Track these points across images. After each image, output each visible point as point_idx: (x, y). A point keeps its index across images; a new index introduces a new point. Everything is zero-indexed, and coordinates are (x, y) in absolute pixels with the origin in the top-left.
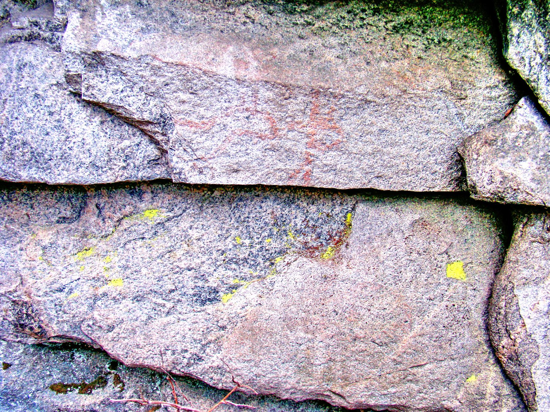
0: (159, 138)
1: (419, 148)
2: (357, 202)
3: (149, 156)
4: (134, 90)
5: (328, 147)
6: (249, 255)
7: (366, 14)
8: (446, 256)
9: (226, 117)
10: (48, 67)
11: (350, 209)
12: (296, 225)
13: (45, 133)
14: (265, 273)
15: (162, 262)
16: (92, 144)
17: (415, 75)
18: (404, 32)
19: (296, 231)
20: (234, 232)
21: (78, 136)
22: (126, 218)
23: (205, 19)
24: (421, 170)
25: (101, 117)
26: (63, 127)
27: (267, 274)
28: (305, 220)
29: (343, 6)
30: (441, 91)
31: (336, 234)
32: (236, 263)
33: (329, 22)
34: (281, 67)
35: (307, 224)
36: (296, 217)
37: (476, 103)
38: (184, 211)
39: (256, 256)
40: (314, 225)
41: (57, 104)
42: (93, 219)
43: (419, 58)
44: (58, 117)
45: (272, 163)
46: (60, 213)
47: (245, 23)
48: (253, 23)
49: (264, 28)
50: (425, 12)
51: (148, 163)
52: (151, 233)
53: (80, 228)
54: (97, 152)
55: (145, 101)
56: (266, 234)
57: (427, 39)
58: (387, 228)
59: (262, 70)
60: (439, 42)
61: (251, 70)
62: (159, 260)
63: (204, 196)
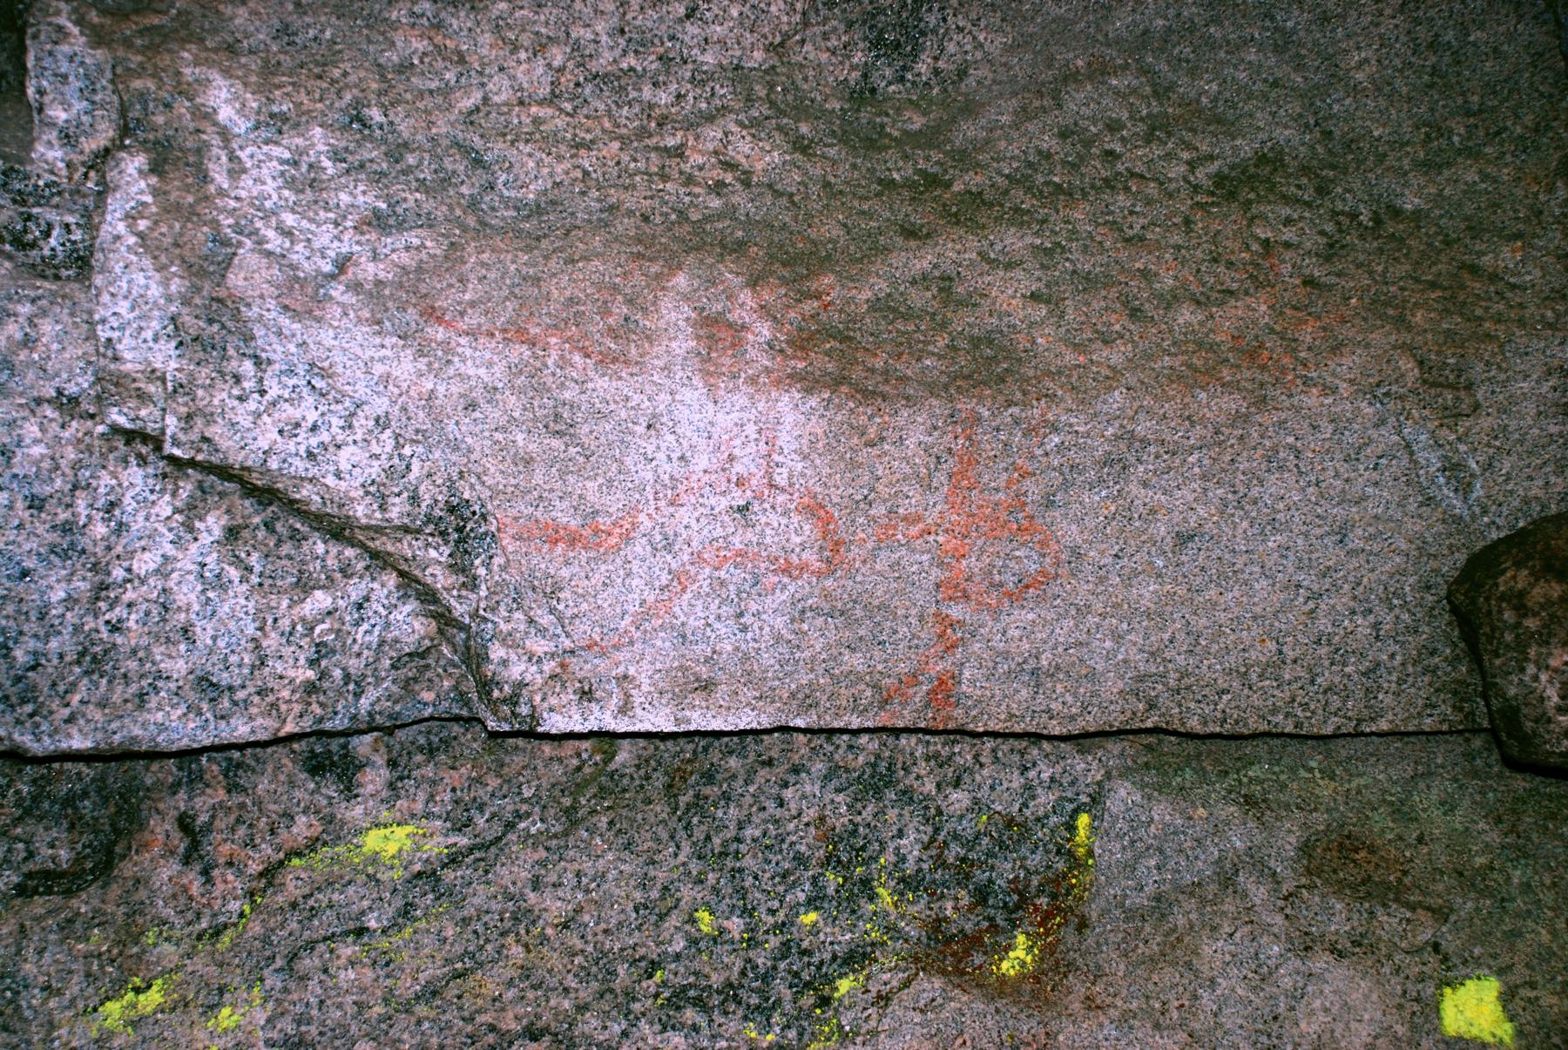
0: (440, 578)
1: (1315, 587)
2: (1108, 776)
3: (396, 641)
4: (355, 423)
5: (1010, 595)
6: (743, 973)
7: (1123, 139)
8: (1433, 960)
9: (672, 510)
10: (19, 336)
11: (1084, 799)
12: (904, 859)
13: (16, 571)
14: (801, 1035)
15: (433, 1014)
16: (196, 607)
17: (1292, 345)
18: (1252, 196)
19: (902, 880)
20: (687, 893)
21: (143, 582)
22: (296, 861)
23: (586, 173)
24: (1327, 663)
25: (228, 511)
26: (83, 551)
27: (806, 1037)
28: (932, 840)
29: (1044, 110)
30: (1387, 394)
31: (1040, 891)
32: (700, 1004)
33: (999, 173)
34: (850, 339)
35: (939, 856)
36: (900, 834)
37: (1513, 424)
38: (510, 826)
39: (766, 978)
40: (963, 860)
41: (57, 468)
42: (168, 871)
43: (1305, 283)
44: (63, 516)
45: (824, 656)
46: (31, 855)
47: (719, 187)
48: (747, 184)
49: (784, 201)
50: (1325, 119)
51: (393, 667)
52: (391, 911)
53: (110, 908)
54: (214, 638)
55: (396, 461)
56: (802, 897)
57: (1334, 213)
58: (1216, 862)
59: (789, 351)
60: (1377, 220)
61: (752, 353)
62: (421, 1010)
63: (579, 769)
